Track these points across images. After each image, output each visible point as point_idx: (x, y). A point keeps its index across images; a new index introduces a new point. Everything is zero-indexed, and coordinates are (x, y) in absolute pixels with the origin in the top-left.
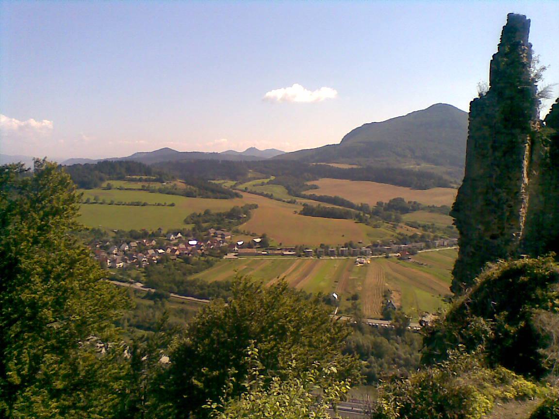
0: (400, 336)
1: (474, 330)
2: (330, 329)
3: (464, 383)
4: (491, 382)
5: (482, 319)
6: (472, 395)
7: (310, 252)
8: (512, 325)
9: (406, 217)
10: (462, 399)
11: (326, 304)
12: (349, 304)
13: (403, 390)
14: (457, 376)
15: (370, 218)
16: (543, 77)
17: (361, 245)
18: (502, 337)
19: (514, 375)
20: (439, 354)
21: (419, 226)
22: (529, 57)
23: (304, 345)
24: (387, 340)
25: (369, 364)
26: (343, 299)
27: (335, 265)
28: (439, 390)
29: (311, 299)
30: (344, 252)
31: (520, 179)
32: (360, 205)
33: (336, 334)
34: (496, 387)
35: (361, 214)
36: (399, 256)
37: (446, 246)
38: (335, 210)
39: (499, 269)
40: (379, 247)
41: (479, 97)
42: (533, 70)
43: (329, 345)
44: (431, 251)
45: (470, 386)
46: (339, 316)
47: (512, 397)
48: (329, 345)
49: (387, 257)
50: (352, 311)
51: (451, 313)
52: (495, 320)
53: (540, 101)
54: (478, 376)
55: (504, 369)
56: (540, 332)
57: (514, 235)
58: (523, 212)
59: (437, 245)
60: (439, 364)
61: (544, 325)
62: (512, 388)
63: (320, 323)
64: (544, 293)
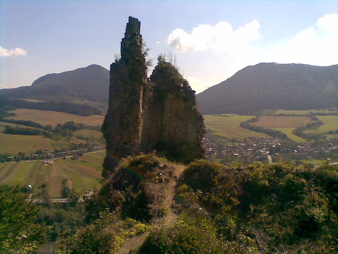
0: (73, 207)
1: (115, 198)
2: (25, 209)
3: (108, 231)
4: (124, 228)
5: (119, 191)
6: (113, 237)
7: (11, 159)
8: (134, 193)
9: (76, 133)
10: (107, 241)
11: (23, 192)
12: (40, 191)
13: (72, 241)
14: (104, 227)
15: (53, 134)
16: (148, 54)
17: (47, 151)
18: (130, 200)
19: (135, 221)
20: (95, 215)
21: (84, 138)
22: (141, 42)
23: (6, 222)
24: (65, 211)
25: (53, 227)
26: (36, 188)
27: (30, 166)
28: (93, 238)
29: (11, 191)
30: (36, 157)
31: (139, 110)
32: (46, 126)
33: (30, 211)
34: (126, 230)
35: (47, 132)
36: (72, 157)
37: (100, 150)
38: (29, 129)
39: (128, 161)
40: (59, 153)
41: (115, 62)
42: (143, 50)
43: (24, 220)
44: (91, 153)
45: (112, 232)
46: (32, 200)
47: (134, 234)
48: (24, 220)
49: (64, 159)
50: (42, 195)
51: (102, 190)
52: (126, 191)
53: (147, 67)
54: (116, 226)
55: (130, 219)
56: (149, 195)
57: (136, 141)
58: (140, 128)
59: (95, 149)
60: (94, 221)
61: (151, 191)
62: (134, 229)
63: (17, 206)
64: (151, 173)
